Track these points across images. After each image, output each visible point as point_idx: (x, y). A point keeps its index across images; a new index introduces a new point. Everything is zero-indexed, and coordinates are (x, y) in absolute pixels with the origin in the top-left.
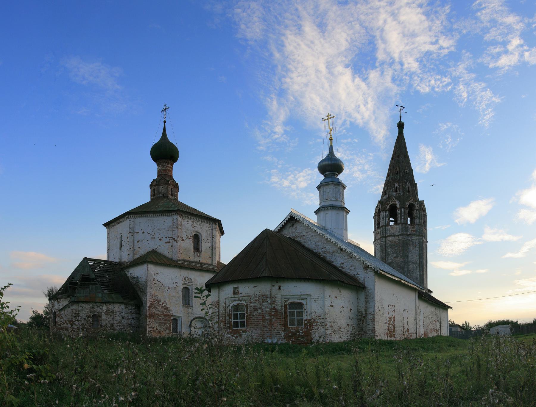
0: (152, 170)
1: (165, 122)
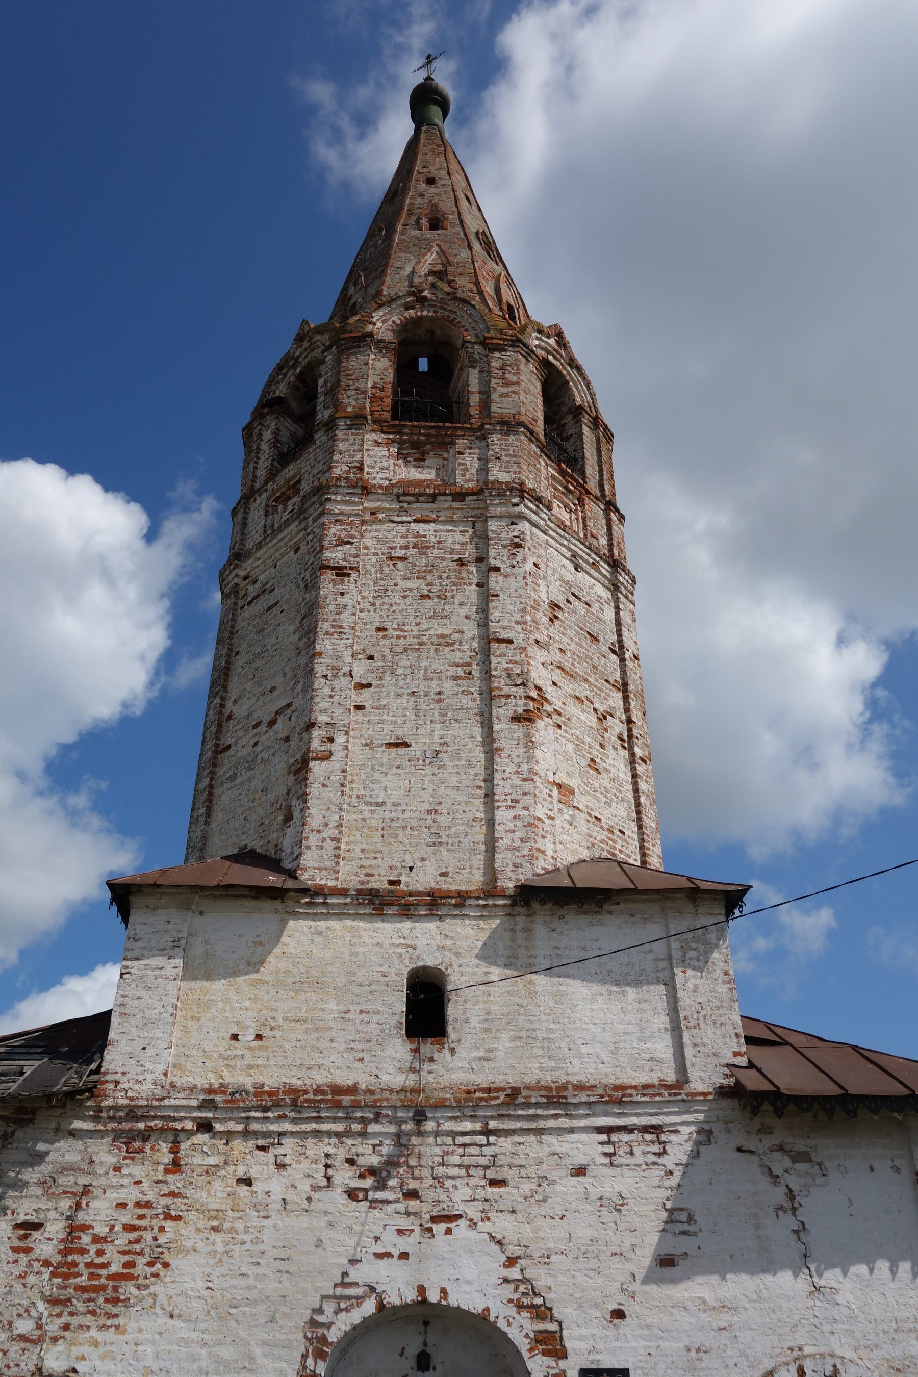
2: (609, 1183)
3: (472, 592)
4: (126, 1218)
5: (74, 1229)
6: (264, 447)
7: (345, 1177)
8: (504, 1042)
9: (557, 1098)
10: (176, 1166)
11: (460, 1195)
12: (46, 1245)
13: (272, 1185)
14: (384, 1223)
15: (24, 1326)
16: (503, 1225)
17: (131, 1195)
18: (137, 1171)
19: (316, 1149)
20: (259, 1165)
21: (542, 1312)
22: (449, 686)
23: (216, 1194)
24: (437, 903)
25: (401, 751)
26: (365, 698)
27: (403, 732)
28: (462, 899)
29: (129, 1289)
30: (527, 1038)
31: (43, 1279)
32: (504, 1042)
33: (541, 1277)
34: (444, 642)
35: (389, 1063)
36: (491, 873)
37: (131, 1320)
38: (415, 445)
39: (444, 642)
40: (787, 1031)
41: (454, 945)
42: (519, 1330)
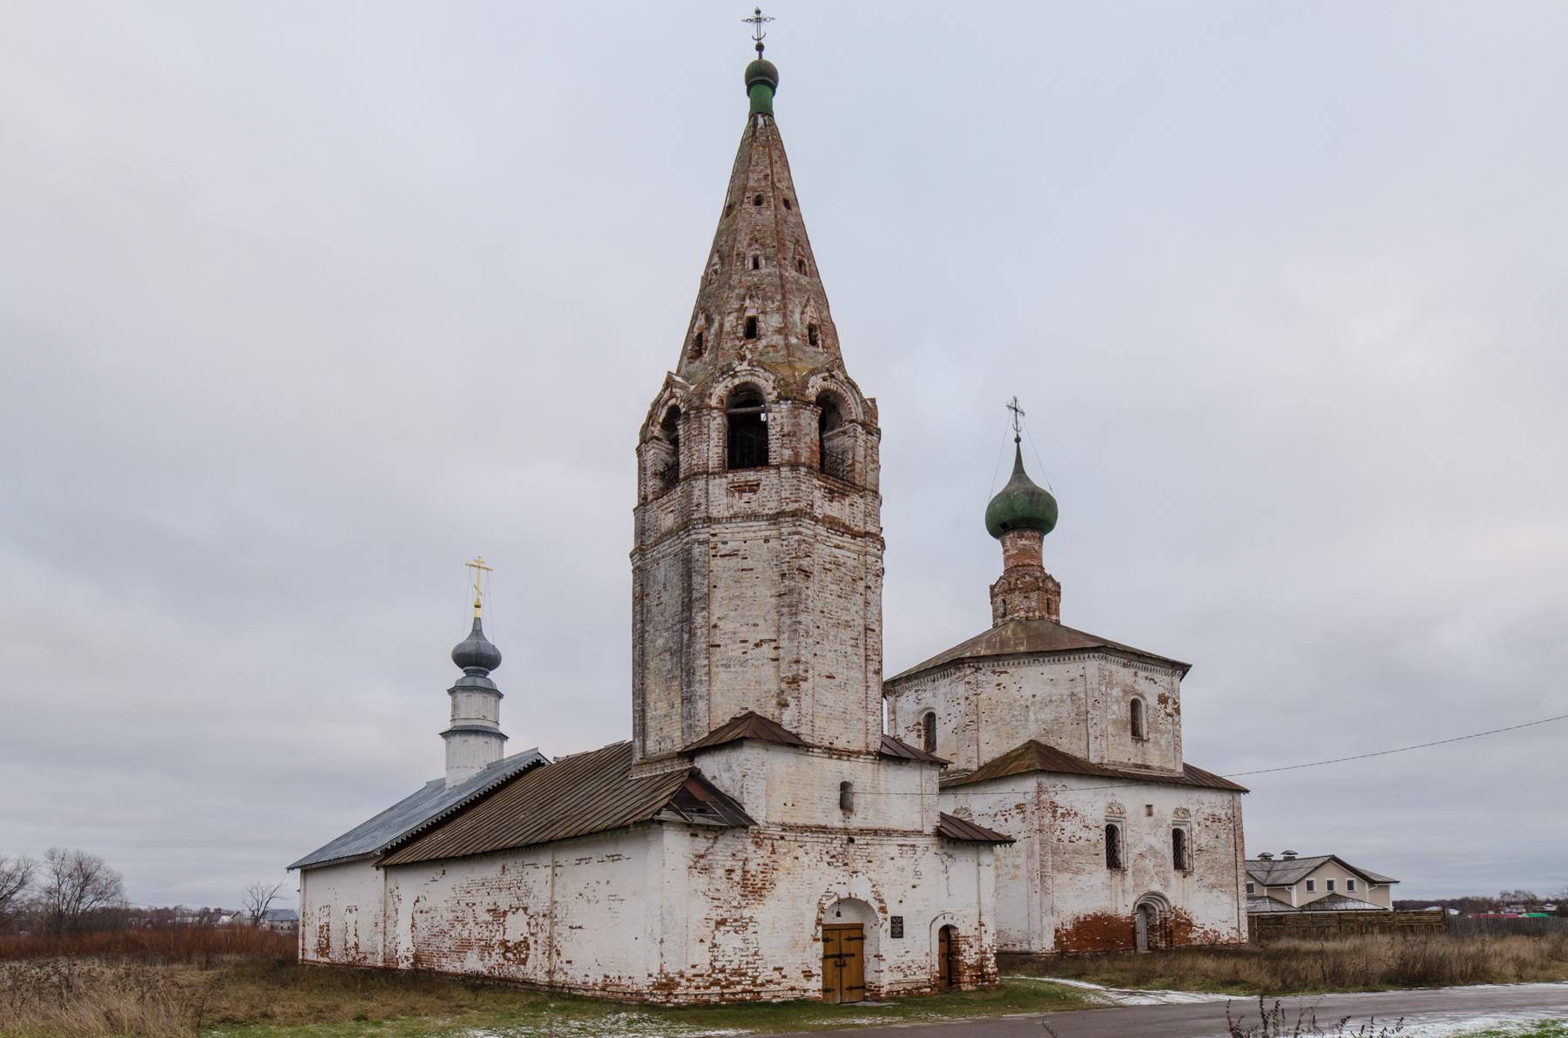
0: (992, 558)
1: (1018, 440)
2: (900, 862)
3: (860, 600)
4: (761, 868)
5: (745, 872)
6: (714, 434)
7: (827, 858)
8: (871, 813)
9: (889, 833)
10: (773, 852)
11: (860, 865)
12: (737, 876)
13: (804, 859)
14: (838, 873)
15: (735, 903)
16: (872, 875)
17: (761, 861)
18: (761, 852)
19: (817, 849)
20: (800, 852)
21: (881, 901)
22: (849, 650)
23: (787, 862)
24: (848, 754)
25: (1127, 837)
26: (817, 649)
27: (832, 670)
28: (859, 753)
29: (764, 892)
30: (877, 811)
31: (738, 889)
32: (871, 813)
33: (882, 891)
34: (847, 625)
35: (835, 819)
36: (867, 745)
37: (766, 901)
38: (831, 491)
39: (847, 625)
40: (482, 811)
41: (862, 773)
42: (875, 905)
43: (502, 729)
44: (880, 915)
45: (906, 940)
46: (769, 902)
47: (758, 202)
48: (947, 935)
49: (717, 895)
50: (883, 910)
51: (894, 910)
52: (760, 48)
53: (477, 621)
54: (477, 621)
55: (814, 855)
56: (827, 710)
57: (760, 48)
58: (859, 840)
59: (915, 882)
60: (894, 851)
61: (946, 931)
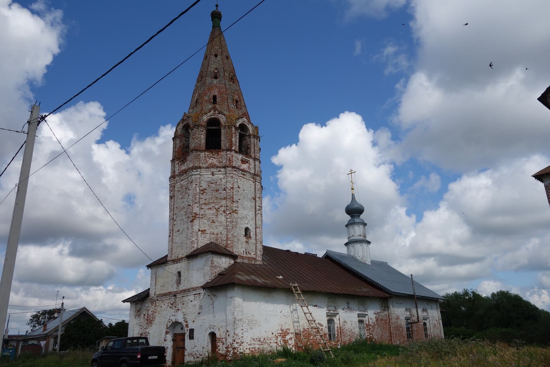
7: (170, 305)
8: (186, 282)
9: (189, 290)
11: (180, 307)
13: (163, 307)
16: (184, 310)
20: (162, 305)
21: (186, 322)
38: (183, 161)
43: (368, 239)
44: (186, 329)
45: (195, 341)
46: (154, 326)
47: (216, 56)
48: (213, 335)
49: (141, 324)
50: (187, 326)
51: (191, 326)
52: (217, 6)
53: (353, 195)
54: (353, 195)
55: (166, 304)
56: (177, 244)
57: (217, 6)
58: (178, 296)
59: (200, 311)
60: (192, 297)
61: (213, 335)
